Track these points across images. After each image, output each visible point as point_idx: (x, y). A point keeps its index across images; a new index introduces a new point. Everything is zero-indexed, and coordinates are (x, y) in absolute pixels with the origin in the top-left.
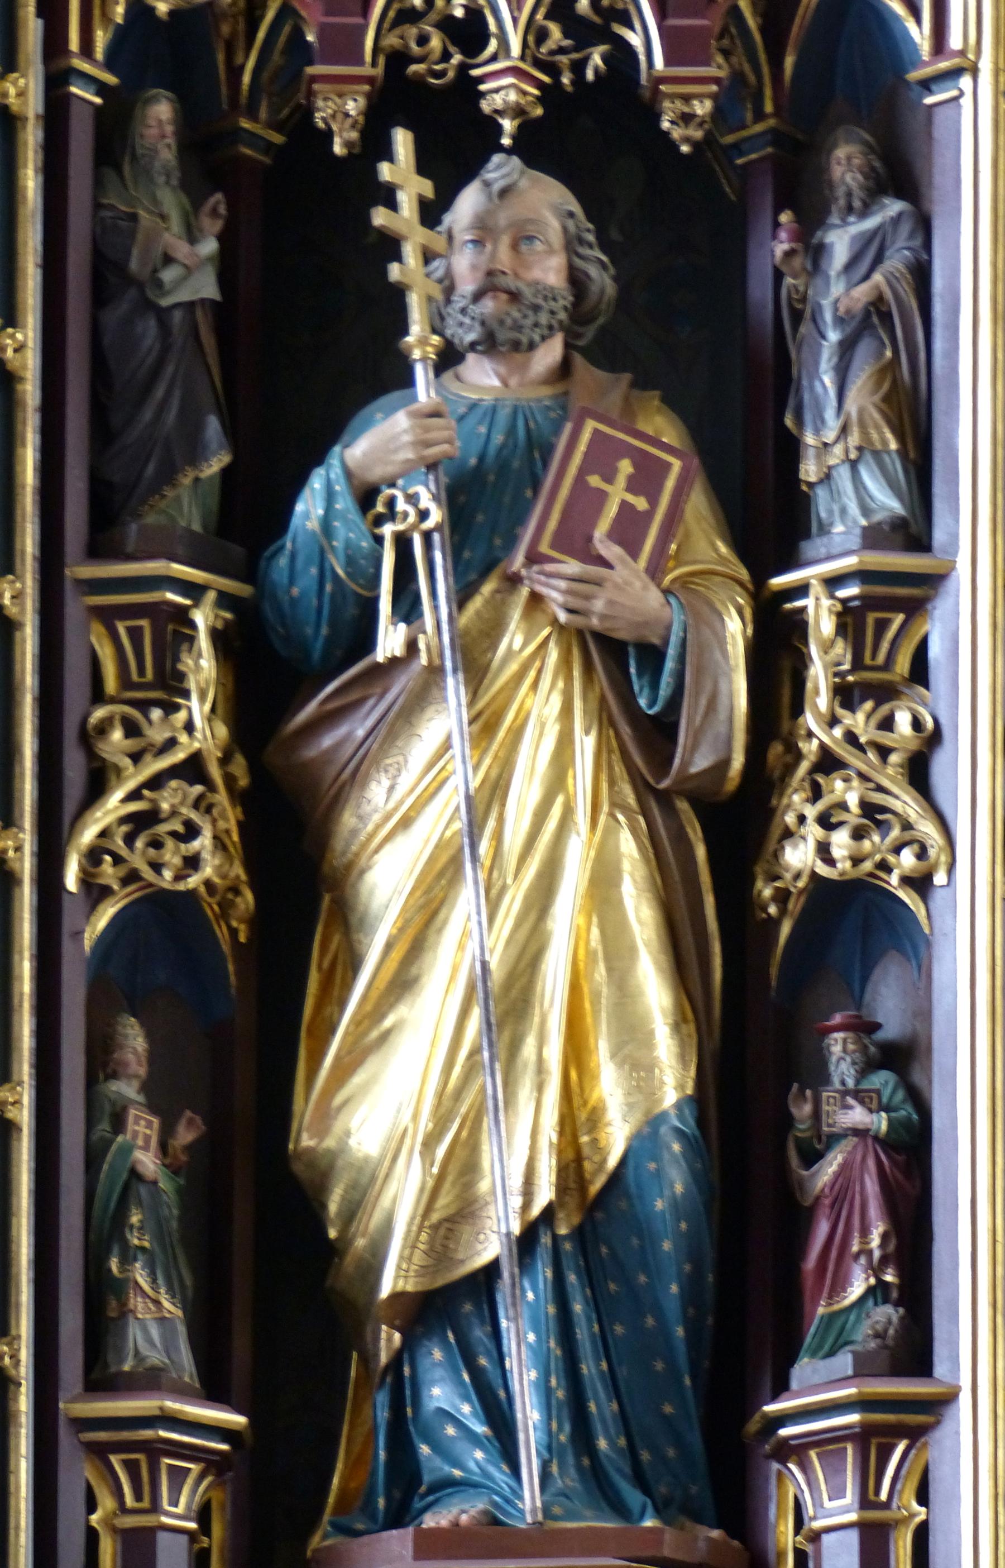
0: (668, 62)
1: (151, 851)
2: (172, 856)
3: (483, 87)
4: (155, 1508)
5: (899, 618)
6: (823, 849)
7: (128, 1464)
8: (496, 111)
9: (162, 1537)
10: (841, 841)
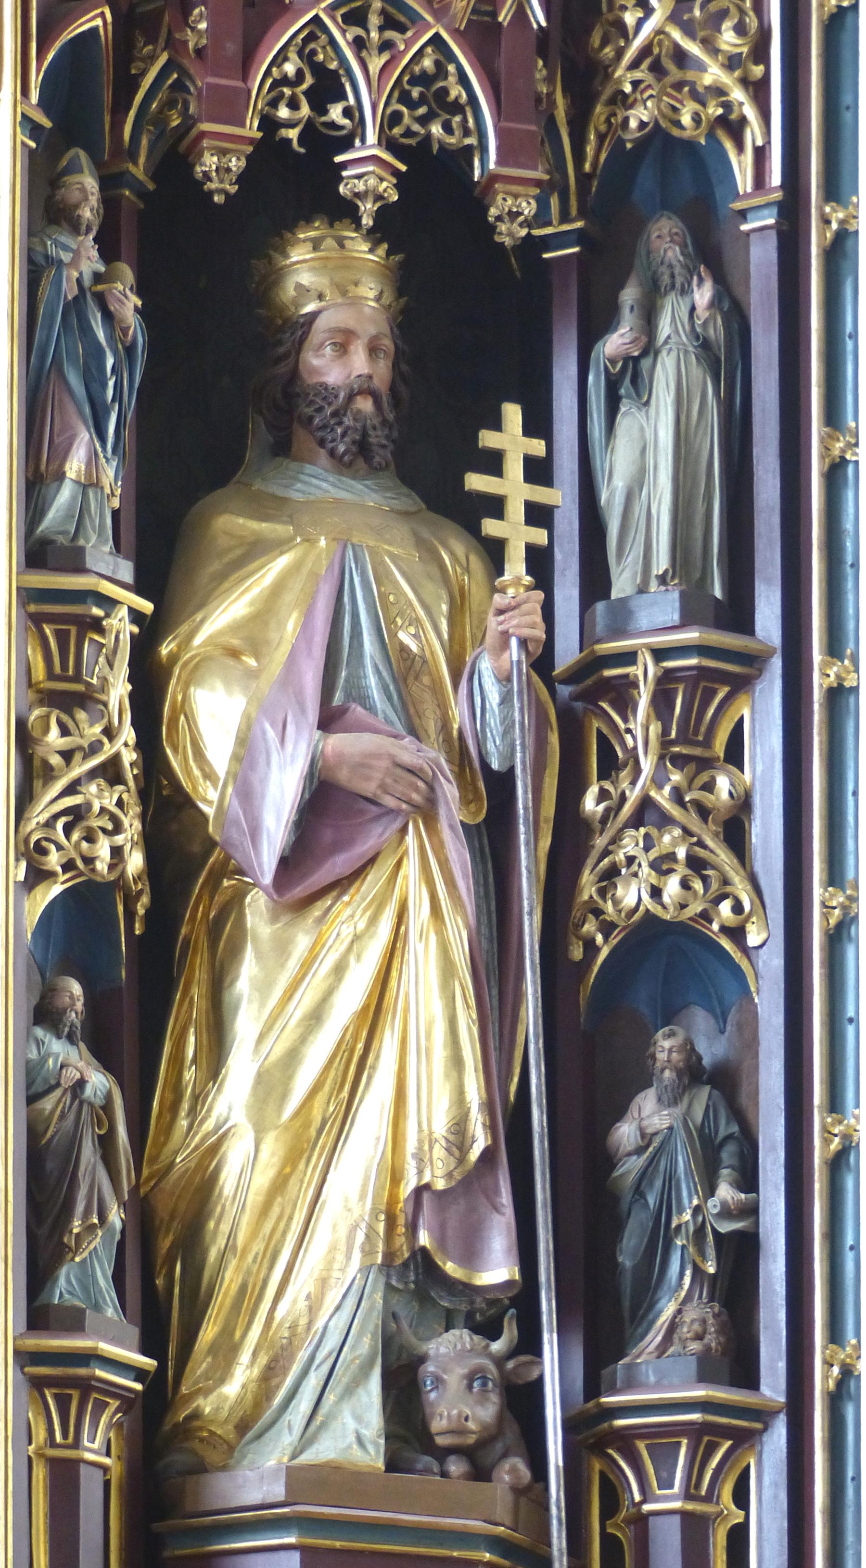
0: (499, 163)
1: (84, 845)
2: (103, 849)
3: (345, 174)
4: (76, 1444)
5: (722, 692)
6: (656, 893)
7: (56, 1397)
8: (357, 195)
9: (83, 1468)
10: (672, 888)
